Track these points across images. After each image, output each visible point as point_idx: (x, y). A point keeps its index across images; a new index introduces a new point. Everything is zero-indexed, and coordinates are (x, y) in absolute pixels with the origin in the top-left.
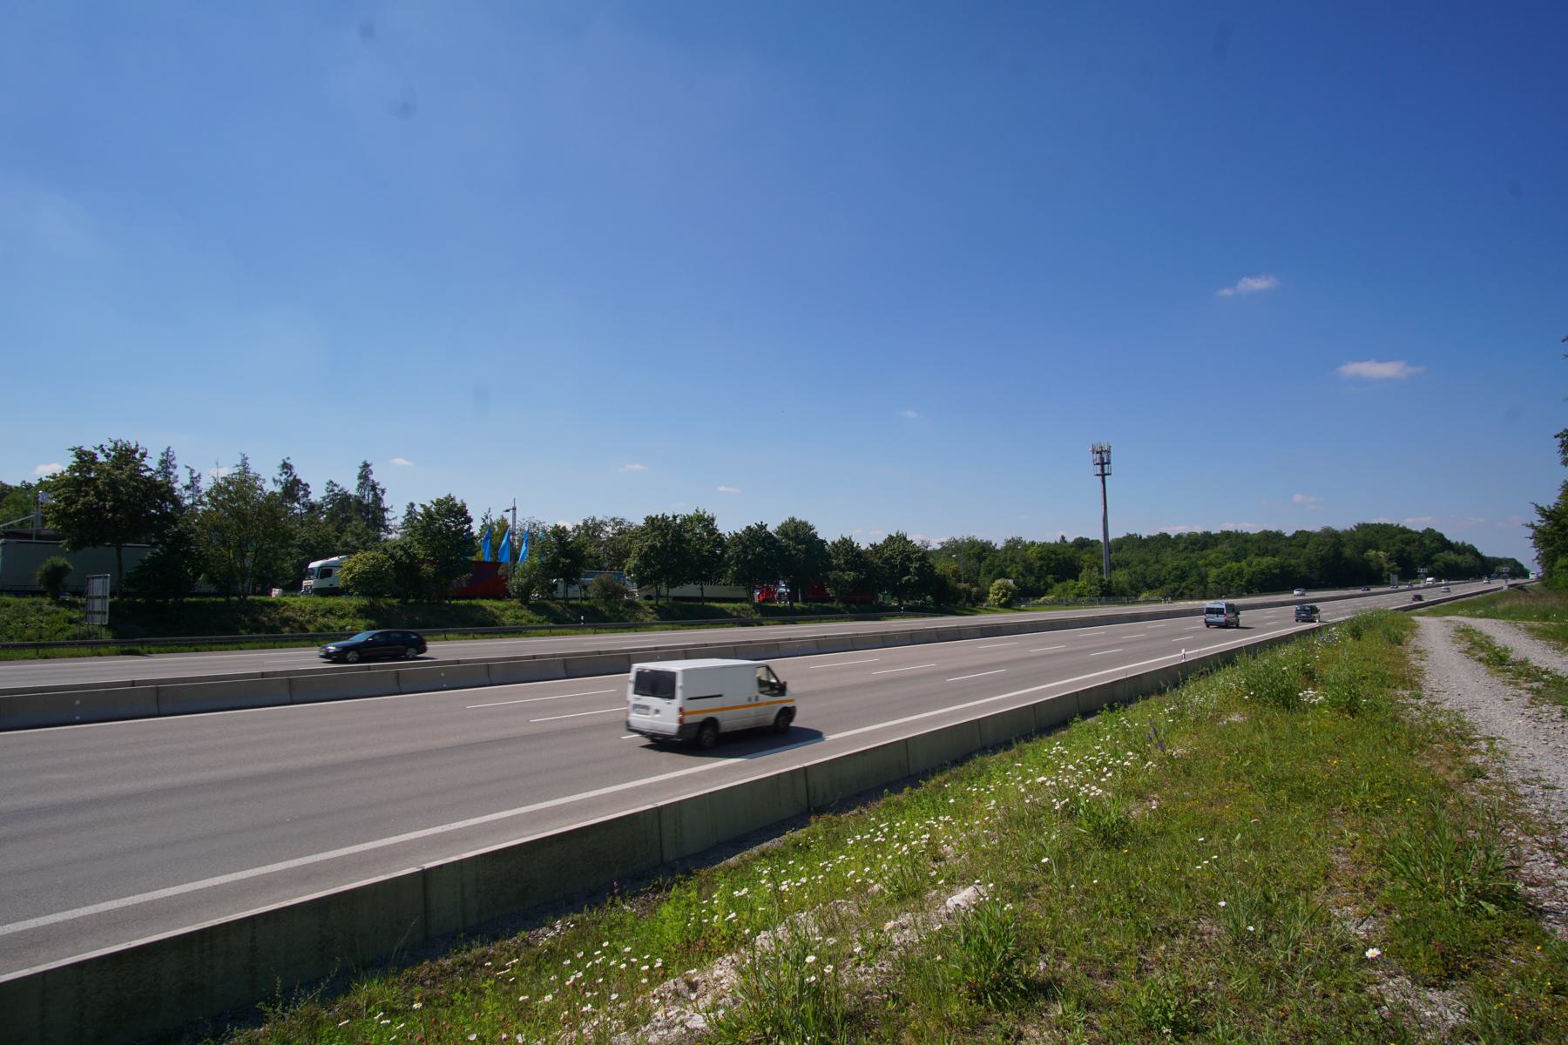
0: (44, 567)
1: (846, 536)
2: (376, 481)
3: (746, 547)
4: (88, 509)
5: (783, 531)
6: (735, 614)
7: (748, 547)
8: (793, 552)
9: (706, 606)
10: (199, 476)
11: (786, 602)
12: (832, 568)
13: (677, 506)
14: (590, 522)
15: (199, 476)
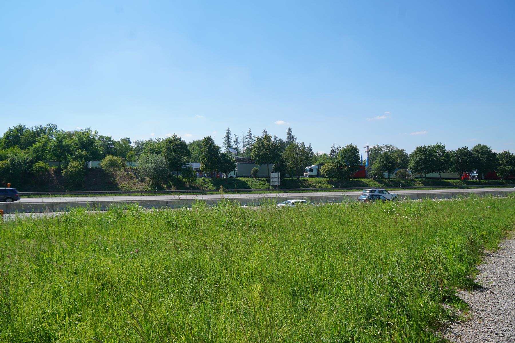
0: (253, 170)
1: (507, 151)
2: (293, 135)
3: (458, 157)
4: (264, 154)
5: (475, 149)
6: (455, 184)
7: (459, 157)
8: (481, 159)
9: (442, 181)
10: (238, 137)
11: (476, 180)
12: (499, 165)
13: (429, 142)
14: (376, 147)
15: (238, 137)
